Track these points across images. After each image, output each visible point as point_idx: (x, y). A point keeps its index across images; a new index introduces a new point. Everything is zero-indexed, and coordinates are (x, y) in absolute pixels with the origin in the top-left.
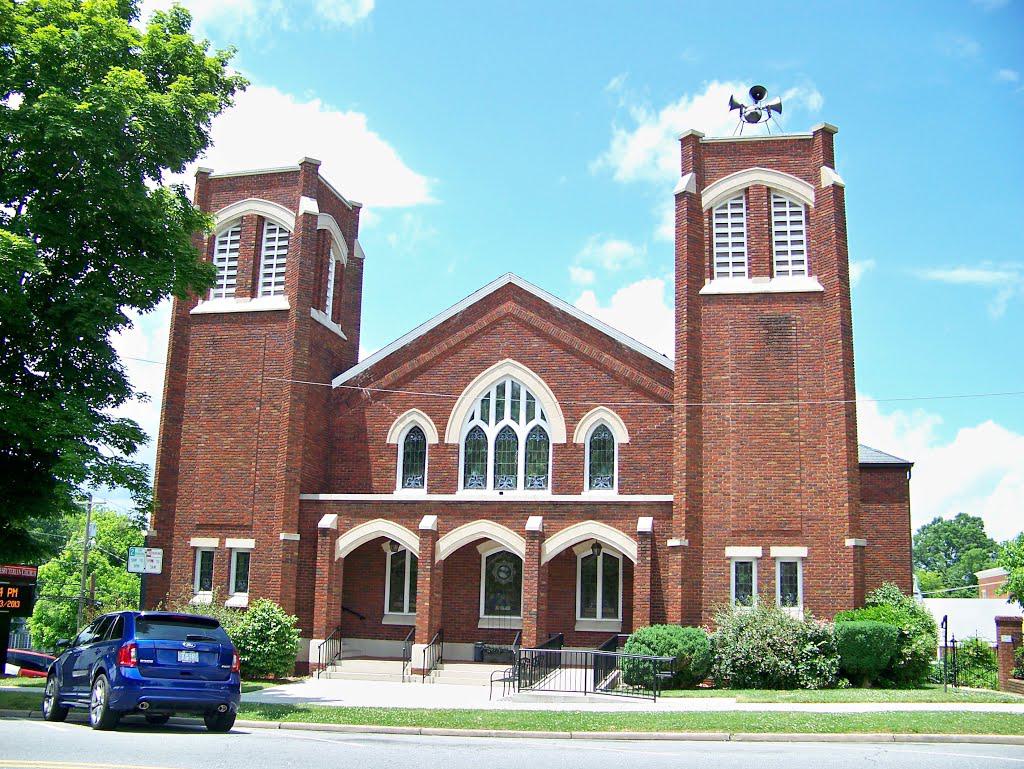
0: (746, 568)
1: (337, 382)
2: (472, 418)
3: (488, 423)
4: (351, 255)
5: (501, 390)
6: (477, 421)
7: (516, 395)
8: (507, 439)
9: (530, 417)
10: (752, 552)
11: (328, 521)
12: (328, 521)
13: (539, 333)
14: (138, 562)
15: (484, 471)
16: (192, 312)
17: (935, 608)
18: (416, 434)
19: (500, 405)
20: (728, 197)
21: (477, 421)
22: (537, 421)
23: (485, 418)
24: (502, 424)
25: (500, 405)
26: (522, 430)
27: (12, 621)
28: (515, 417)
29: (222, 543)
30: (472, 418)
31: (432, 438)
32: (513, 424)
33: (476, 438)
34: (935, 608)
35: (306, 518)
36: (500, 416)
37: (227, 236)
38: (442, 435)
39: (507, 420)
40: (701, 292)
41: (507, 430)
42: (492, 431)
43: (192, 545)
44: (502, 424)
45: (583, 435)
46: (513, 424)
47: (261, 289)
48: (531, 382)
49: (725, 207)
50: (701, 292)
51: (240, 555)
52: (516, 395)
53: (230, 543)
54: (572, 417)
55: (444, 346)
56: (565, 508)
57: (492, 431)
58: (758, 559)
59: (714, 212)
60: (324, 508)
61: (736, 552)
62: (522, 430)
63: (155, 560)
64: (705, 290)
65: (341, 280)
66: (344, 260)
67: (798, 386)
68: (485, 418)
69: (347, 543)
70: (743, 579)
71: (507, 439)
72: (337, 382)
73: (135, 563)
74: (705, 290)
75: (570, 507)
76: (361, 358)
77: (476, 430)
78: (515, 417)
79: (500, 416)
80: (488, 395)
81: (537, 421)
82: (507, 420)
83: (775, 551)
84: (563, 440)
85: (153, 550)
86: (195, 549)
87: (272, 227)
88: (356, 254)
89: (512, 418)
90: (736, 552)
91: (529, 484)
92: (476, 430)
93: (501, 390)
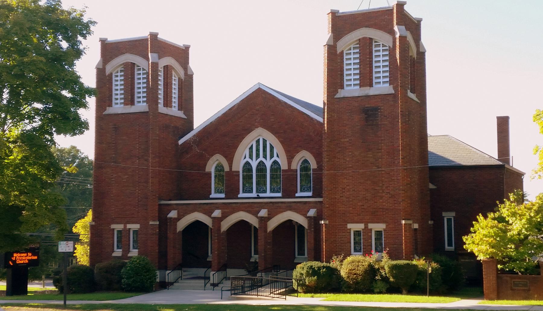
0: (359, 234)
1: (181, 142)
2: (245, 158)
3: (252, 160)
4: (186, 74)
5: (258, 142)
6: (248, 159)
8: (261, 167)
9: (272, 156)
10: (360, 227)
11: (173, 214)
12: (173, 214)
14: (62, 248)
16: (104, 113)
18: (219, 168)
19: (258, 150)
20: (351, 44)
21: (248, 159)
23: (251, 157)
25: (258, 150)
26: (268, 163)
27: (29, 269)
28: (265, 157)
29: (125, 226)
30: (245, 158)
31: (227, 169)
32: (264, 160)
33: (247, 167)
35: (162, 211)
36: (258, 156)
37: (118, 72)
38: (231, 167)
39: (261, 158)
40: (335, 97)
42: (254, 164)
43: (111, 228)
44: (259, 160)
45: (296, 165)
46: (264, 160)
47: (136, 100)
48: (272, 139)
49: (350, 49)
50: (335, 97)
51: (134, 231)
53: (129, 226)
54: (290, 159)
56: (277, 205)
57: (254, 164)
58: (363, 229)
59: (345, 52)
60: (170, 208)
61: (354, 227)
62: (268, 163)
63: (70, 246)
64: (338, 96)
65: (182, 87)
66: (182, 76)
67: (381, 143)
68: (251, 157)
69: (182, 225)
70: (357, 239)
71: (261, 167)
72: (181, 142)
73: (61, 248)
74: (338, 96)
75: (280, 205)
76: (195, 127)
77: (247, 163)
78: (265, 157)
79: (258, 156)
80: (252, 146)
82: (261, 158)
83: (370, 226)
84: (287, 168)
85: (69, 242)
86: (114, 229)
87: (139, 68)
88: (189, 73)
90: (354, 227)
91: (272, 191)
92: (247, 163)
93: (258, 142)
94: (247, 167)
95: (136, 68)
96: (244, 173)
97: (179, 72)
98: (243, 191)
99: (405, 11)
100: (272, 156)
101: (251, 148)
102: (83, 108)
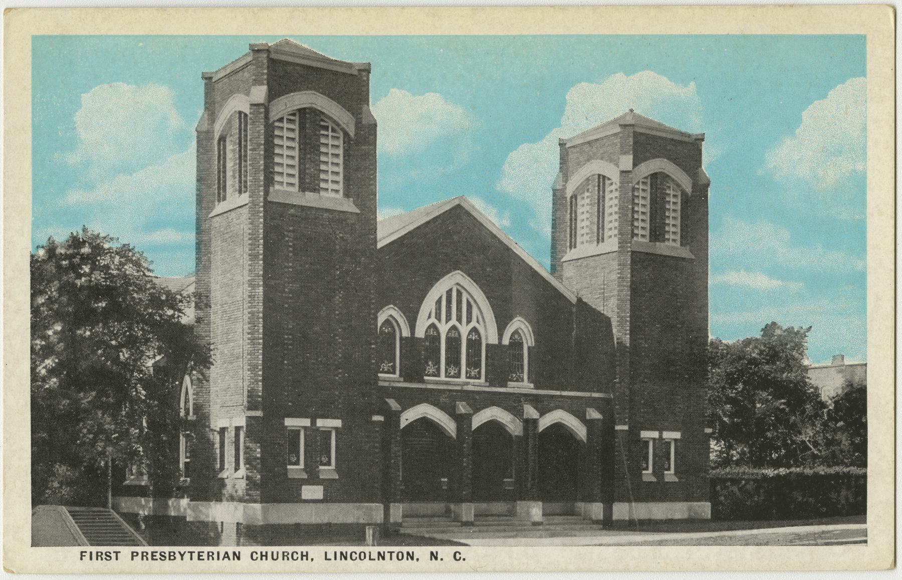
2: (429, 317)
7: (459, 294)
8: (453, 343)
9: (469, 321)
13: (599, 189)
15: (437, 362)
17: (403, 212)
21: (433, 320)
22: (473, 324)
23: (438, 317)
24: (450, 324)
26: (464, 330)
28: (459, 319)
30: (429, 317)
34: (403, 212)
36: (449, 318)
38: (412, 328)
39: (454, 321)
41: (454, 328)
42: (444, 328)
46: (457, 324)
52: (459, 294)
55: (601, 184)
57: (444, 328)
68: (438, 317)
71: (453, 343)
77: (433, 326)
78: (459, 319)
79: (449, 318)
80: (441, 297)
81: (473, 324)
82: (454, 321)
89: (457, 320)
94: (433, 337)
95: (607, 182)
96: (38, 342)
97: (630, 544)
98: (466, 376)
99: (705, 509)
100: (469, 321)
101: (439, 302)
102: (748, 342)
